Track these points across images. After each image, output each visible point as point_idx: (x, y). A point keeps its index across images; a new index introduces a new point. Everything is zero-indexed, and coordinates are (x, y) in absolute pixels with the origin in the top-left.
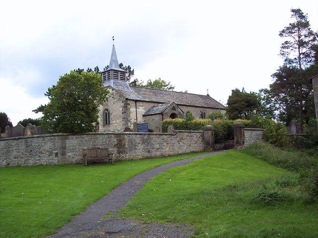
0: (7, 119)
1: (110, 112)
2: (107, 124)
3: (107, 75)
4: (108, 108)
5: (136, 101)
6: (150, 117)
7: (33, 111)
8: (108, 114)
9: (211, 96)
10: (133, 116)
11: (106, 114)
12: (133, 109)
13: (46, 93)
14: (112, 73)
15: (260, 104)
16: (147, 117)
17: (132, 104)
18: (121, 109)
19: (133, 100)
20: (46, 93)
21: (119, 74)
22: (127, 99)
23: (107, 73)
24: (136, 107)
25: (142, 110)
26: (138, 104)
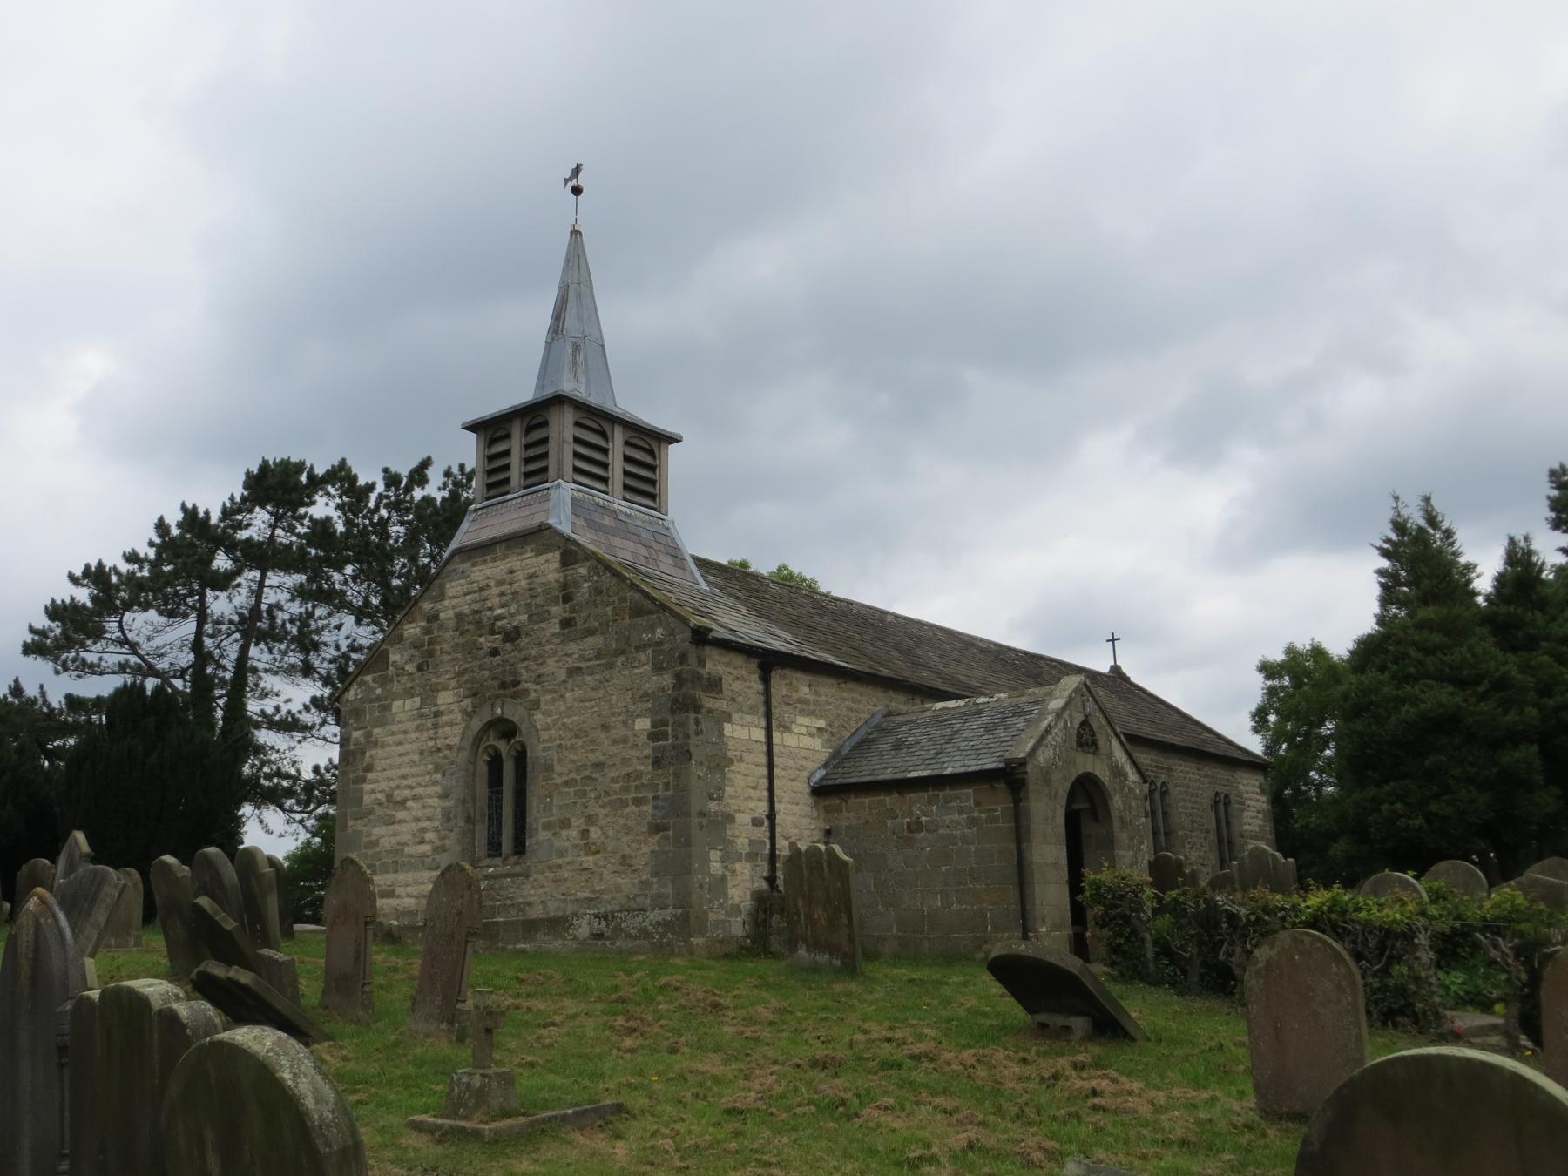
0: (1369, 636)
1: (538, 751)
2: (494, 849)
3: (516, 443)
4: (512, 711)
5: (768, 662)
6: (889, 800)
7: (41, 687)
8: (508, 768)
9: (1135, 678)
10: (743, 794)
11: (495, 764)
12: (744, 732)
13: (455, 470)
14: (563, 427)
15: (360, 801)
16: (854, 801)
17: (741, 680)
18: (643, 724)
19: (748, 651)
20: (455, 470)
21: (619, 436)
22: (701, 637)
23: (517, 431)
24: (768, 716)
25: (805, 743)
26: (782, 684)
